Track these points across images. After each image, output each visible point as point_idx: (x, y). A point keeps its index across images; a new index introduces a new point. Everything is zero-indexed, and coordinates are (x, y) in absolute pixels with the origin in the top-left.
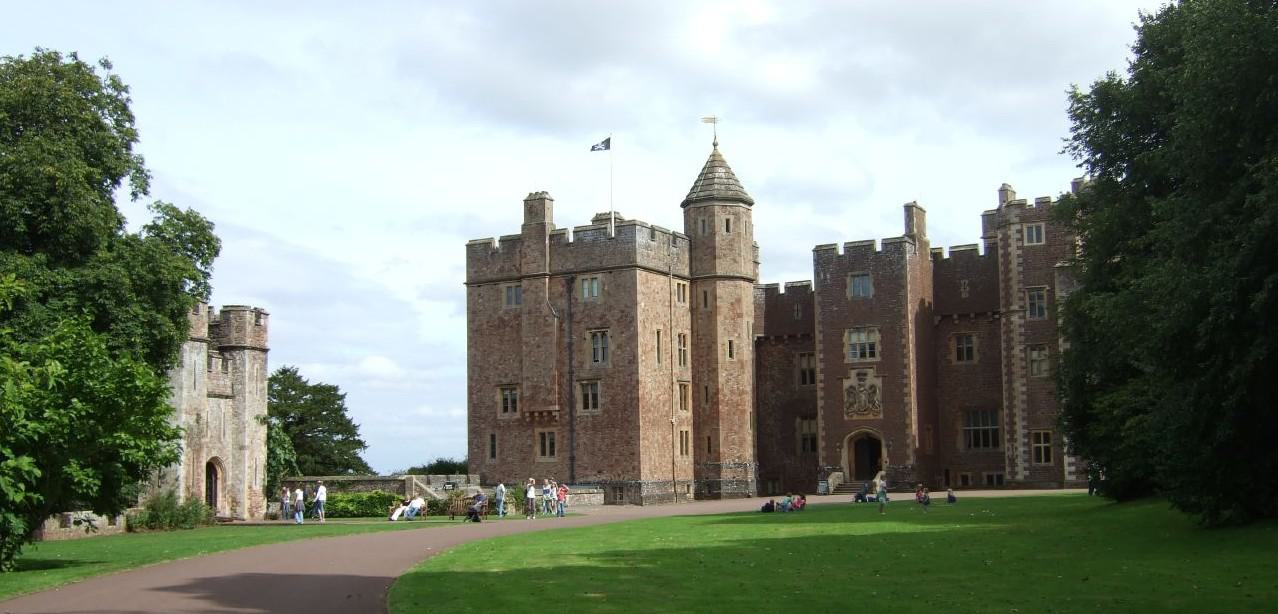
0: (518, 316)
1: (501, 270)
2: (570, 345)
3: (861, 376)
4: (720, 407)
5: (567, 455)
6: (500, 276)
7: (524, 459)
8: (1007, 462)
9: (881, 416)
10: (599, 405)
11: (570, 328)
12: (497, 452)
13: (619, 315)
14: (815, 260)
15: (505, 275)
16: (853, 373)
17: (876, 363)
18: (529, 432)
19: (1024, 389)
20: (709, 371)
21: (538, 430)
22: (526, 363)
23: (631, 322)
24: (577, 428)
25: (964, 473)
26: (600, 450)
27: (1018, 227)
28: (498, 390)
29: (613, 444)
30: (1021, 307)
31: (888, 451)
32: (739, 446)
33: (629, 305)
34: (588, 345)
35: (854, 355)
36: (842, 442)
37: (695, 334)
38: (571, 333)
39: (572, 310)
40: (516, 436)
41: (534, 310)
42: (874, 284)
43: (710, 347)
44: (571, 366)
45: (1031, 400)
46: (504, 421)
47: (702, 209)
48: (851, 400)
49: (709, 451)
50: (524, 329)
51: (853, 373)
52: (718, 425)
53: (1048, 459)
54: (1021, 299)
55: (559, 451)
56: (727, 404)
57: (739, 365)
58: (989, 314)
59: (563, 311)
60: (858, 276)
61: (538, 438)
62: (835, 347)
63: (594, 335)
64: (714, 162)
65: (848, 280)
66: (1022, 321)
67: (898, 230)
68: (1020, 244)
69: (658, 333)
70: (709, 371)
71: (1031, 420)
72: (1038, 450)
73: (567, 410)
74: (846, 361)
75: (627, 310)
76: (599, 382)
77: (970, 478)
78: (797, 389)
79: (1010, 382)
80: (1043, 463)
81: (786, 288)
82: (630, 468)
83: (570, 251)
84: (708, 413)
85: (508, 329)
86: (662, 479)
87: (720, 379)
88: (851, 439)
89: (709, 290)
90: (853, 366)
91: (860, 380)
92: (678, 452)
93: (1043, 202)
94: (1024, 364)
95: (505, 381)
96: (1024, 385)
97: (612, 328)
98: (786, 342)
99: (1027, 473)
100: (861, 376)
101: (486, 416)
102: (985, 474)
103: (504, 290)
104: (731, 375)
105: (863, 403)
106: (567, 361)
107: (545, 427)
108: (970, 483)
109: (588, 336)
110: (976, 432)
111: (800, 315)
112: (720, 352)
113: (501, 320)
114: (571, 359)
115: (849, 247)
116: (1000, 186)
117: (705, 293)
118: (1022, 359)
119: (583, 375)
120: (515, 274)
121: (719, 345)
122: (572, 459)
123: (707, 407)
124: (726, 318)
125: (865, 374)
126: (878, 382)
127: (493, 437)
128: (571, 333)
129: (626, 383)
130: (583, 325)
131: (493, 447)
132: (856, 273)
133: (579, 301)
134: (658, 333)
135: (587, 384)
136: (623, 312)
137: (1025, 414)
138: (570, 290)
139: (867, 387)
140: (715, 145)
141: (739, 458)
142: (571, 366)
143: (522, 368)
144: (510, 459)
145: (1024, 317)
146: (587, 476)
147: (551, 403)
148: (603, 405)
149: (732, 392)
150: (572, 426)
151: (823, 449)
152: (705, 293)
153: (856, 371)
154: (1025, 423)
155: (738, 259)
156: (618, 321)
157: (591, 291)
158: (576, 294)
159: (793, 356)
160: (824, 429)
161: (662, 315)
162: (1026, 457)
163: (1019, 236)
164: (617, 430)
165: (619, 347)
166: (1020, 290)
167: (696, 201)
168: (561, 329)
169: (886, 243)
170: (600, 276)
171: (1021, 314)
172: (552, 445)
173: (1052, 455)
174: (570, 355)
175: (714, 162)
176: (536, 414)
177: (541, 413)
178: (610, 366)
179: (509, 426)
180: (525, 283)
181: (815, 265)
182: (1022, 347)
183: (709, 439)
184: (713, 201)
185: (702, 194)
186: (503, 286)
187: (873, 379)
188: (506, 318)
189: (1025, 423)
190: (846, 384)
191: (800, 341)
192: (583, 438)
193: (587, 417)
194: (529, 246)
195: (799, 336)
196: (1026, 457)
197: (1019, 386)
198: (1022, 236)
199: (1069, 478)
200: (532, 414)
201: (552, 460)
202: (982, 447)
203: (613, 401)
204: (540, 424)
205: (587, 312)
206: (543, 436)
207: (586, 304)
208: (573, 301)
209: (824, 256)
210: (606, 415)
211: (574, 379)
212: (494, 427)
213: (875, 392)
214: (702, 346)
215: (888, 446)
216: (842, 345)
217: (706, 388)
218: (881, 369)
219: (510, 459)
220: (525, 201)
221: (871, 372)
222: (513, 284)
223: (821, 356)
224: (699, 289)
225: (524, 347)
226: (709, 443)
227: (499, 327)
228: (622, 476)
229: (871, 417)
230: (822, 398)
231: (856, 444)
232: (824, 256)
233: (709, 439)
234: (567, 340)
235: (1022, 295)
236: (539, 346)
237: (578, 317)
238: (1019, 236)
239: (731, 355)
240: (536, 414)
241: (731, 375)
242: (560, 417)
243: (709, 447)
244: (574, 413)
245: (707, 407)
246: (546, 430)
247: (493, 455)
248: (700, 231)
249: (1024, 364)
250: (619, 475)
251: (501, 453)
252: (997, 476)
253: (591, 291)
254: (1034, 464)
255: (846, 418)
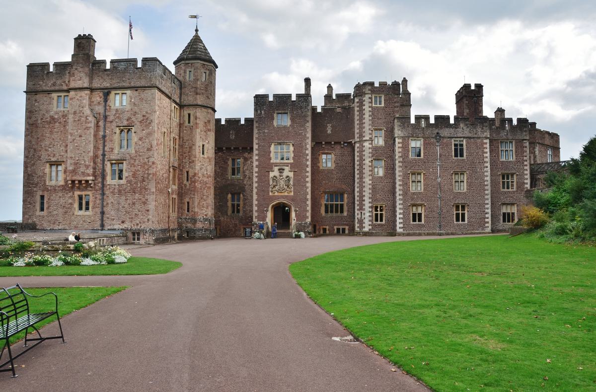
0: (64, 116)
1: (54, 84)
2: (104, 137)
3: (281, 170)
4: (196, 184)
5: (98, 210)
6: (53, 88)
7: (66, 212)
8: (356, 221)
9: (292, 194)
10: (124, 177)
11: (105, 125)
12: (201, 147)
13: (142, 118)
14: (255, 103)
15: (57, 88)
16: (276, 169)
17: (290, 163)
18: (71, 194)
19: (371, 182)
20: (190, 162)
21: (77, 193)
22: (70, 147)
23: (150, 123)
24: (107, 192)
25: (325, 227)
26: (123, 207)
27: (370, 96)
28: (48, 165)
29: (134, 204)
30: (370, 138)
31: (296, 214)
32: (204, 208)
33: (149, 112)
34: (116, 137)
35: (276, 158)
36: (268, 207)
37: (181, 139)
38: (105, 128)
39: (107, 113)
40: (60, 197)
41: (78, 112)
42: (291, 119)
43: (191, 148)
44: (104, 151)
45: (374, 189)
46: (51, 186)
47: (190, 65)
48: (275, 184)
49: (188, 211)
50: (70, 124)
51: (276, 169)
52: (194, 195)
53: (381, 220)
54: (370, 134)
55: (93, 208)
56: (201, 183)
57: (208, 160)
58: (342, 143)
59: (100, 114)
60: (281, 113)
61: (77, 198)
62: (265, 154)
63: (122, 131)
64: (196, 40)
65: (275, 115)
66: (371, 146)
67: (302, 91)
68: (371, 105)
69: (164, 133)
70: (190, 162)
71: (373, 198)
72: (376, 215)
73: (100, 180)
74: (272, 161)
75: (148, 115)
76: (124, 162)
77: (327, 229)
78: (229, 178)
79: (361, 178)
80: (379, 222)
81: (226, 120)
82: (146, 220)
83: (107, 74)
84: (188, 187)
85: (57, 124)
86: (164, 227)
87: (197, 167)
88: (273, 206)
89: (192, 113)
90: (276, 165)
91: (281, 172)
92: (171, 211)
93: (383, 85)
94: (371, 168)
95: (53, 159)
96: (370, 180)
97: (136, 126)
98: (224, 151)
99: (370, 227)
100: (281, 170)
101: (38, 183)
102: (335, 227)
103: (56, 98)
104: (203, 165)
105: (282, 186)
106: (101, 148)
107: (82, 191)
108: (327, 232)
109: (118, 131)
110: (332, 206)
111: (233, 137)
112: (197, 151)
113: (52, 118)
114: (104, 146)
115: (228, 121)
116: (328, 85)
117: (189, 115)
118: (369, 166)
119: (113, 157)
120: (65, 88)
121: (197, 147)
122: (103, 213)
123: (188, 184)
124: (201, 131)
125: (283, 170)
126: (291, 175)
127: (42, 197)
128: (105, 128)
129: (145, 163)
130: (114, 124)
131: (42, 204)
132: (280, 112)
133: (112, 108)
134: (164, 133)
135: (115, 164)
136: (144, 116)
137: (371, 196)
138: (106, 100)
139: (284, 177)
140: (197, 31)
141: (206, 215)
142: (104, 151)
143: (66, 151)
144: (55, 212)
145: (372, 144)
146: (114, 225)
147: (88, 175)
148: (127, 177)
149: (203, 175)
150: (103, 190)
151: (256, 211)
152: (189, 115)
153: (278, 167)
154: (370, 200)
155: (210, 97)
156: (140, 122)
157: (121, 102)
158: (110, 103)
159: (228, 159)
160: (257, 200)
161: (167, 123)
162: (370, 218)
163: (370, 100)
164: (137, 194)
165: (140, 139)
166: (370, 129)
167: (187, 59)
168: (97, 126)
169: (246, 120)
170: (128, 92)
171: (370, 142)
172: (87, 203)
173: (384, 218)
174: (104, 143)
175: (196, 40)
176: (77, 182)
177: (80, 182)
178: (133, 152)
179: (55, 190)
180: (72, 93)
181: (255, 106)
182: (370, 159)
183: (188, 203)
184: (196, 55)
185: (190, 56)
186: (55, 95)
187: (287, 172)
188: (56, 117)
189: (370, 200)
190: (272, 174)
191: (232, 152)
192: (110, 199)
193: (115, 185)
194: (76, 69)
195: (232, 148)
196: (370, 218)
197: (367, 181)
198: (372, 101)
199: (399, 230)
200: (73, 182)
201: (87, 213)
202: (334, 213)
203: (134, 175)
204: (79, 188)
205: (117, 115)
206: (81, 198)
207: (117, 110)
208: (108, 107)
209: (260, 100)
210: (129, 185)
211: (106, 160)
212: (43, 191)
213: (289, 180)
214: (186, 146)
215: (296, 211)
216: (270, 152)
217: (188, 172)
218: (293, 166)
219: (55, 212)
220: (75, 39)
221: (287, 169)
222: (62, 94)
223: (257, 158)
224: (185, 112)
225: (70, 137)
226: (188, 206)
227: (50, 122)
228: (140, 225)
229: (286, 194)
230: (256, 182)
231: (274, 209)
232: (260, 100)
233: (188, 203)
234: (101, 133)
235: (371, 132)
236: (80, 136)
237: (111, 118)
238: (370, 100)
239: (203, 154)
240: (77, 182)
241: (203, 165)
242: (95, 184)
243: (188, 209)
244: (105, 183)
245: (188, 184)
246: (83, 193)
247: (42, 209)
248: (187, 78)
249: (371, 168)
250: (137, 224)
251: (48, 208)
252: (342, 229)
253: (121, 102)
254: (374, 222)
255: (271, 194)
